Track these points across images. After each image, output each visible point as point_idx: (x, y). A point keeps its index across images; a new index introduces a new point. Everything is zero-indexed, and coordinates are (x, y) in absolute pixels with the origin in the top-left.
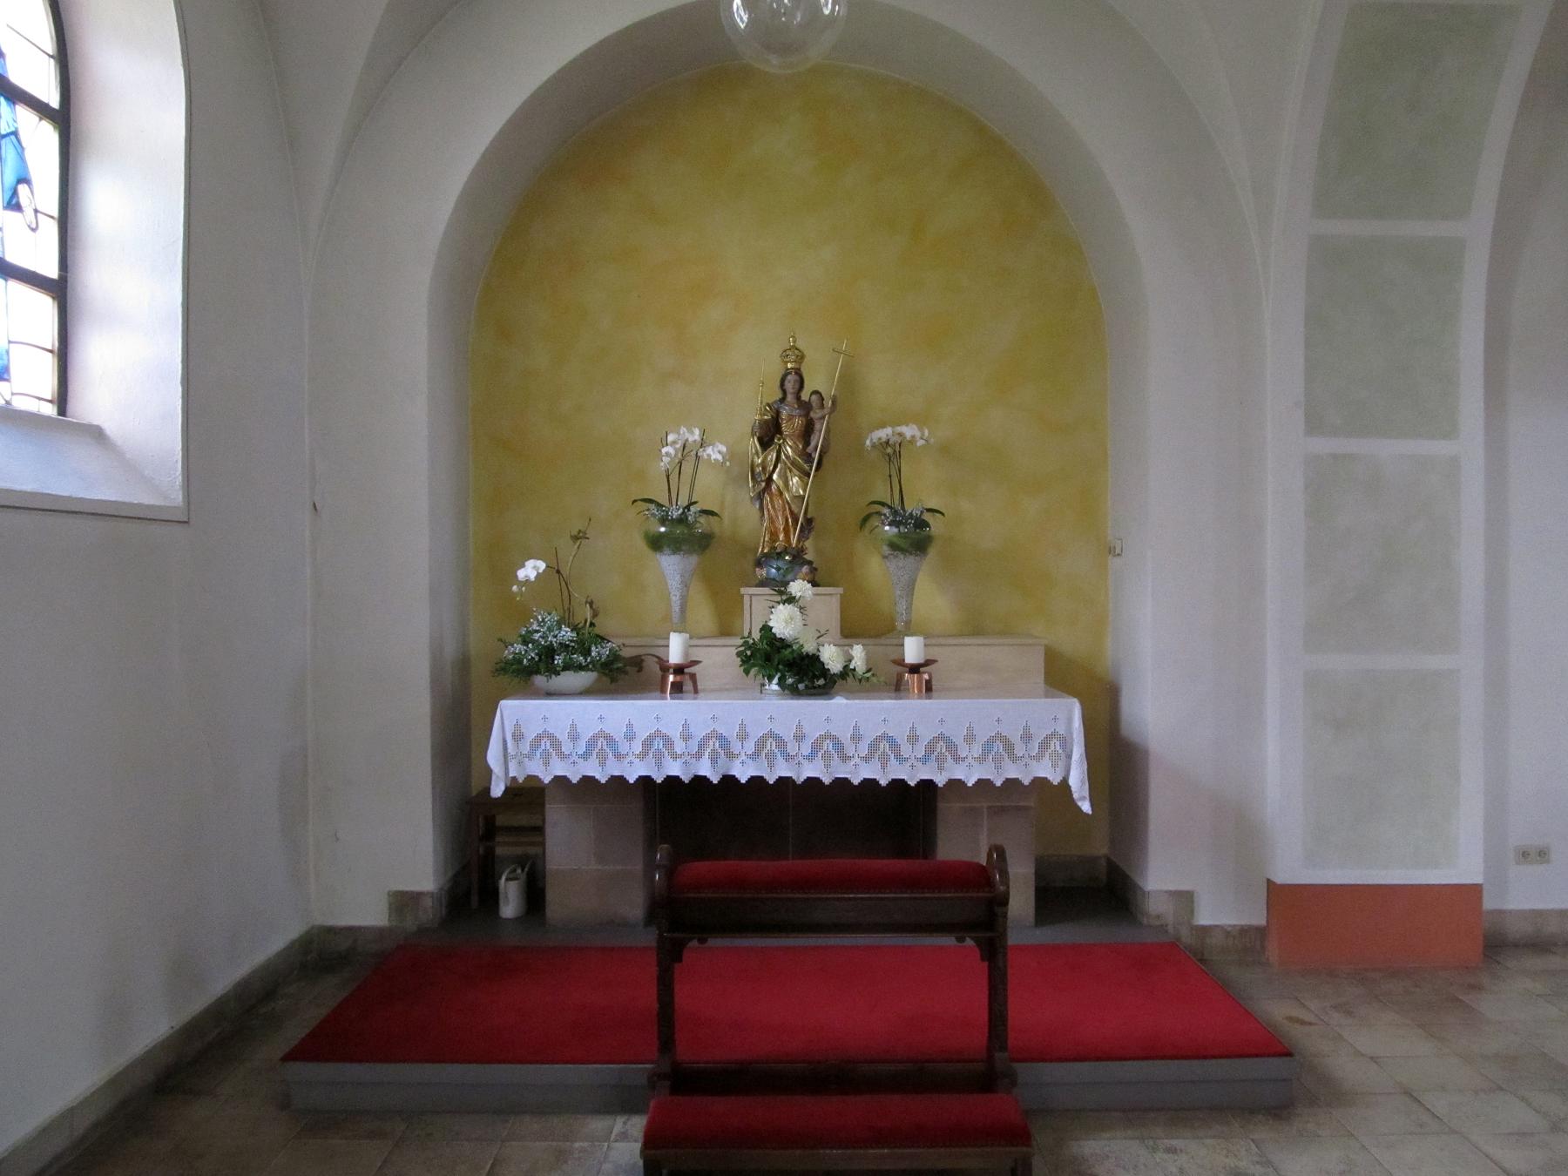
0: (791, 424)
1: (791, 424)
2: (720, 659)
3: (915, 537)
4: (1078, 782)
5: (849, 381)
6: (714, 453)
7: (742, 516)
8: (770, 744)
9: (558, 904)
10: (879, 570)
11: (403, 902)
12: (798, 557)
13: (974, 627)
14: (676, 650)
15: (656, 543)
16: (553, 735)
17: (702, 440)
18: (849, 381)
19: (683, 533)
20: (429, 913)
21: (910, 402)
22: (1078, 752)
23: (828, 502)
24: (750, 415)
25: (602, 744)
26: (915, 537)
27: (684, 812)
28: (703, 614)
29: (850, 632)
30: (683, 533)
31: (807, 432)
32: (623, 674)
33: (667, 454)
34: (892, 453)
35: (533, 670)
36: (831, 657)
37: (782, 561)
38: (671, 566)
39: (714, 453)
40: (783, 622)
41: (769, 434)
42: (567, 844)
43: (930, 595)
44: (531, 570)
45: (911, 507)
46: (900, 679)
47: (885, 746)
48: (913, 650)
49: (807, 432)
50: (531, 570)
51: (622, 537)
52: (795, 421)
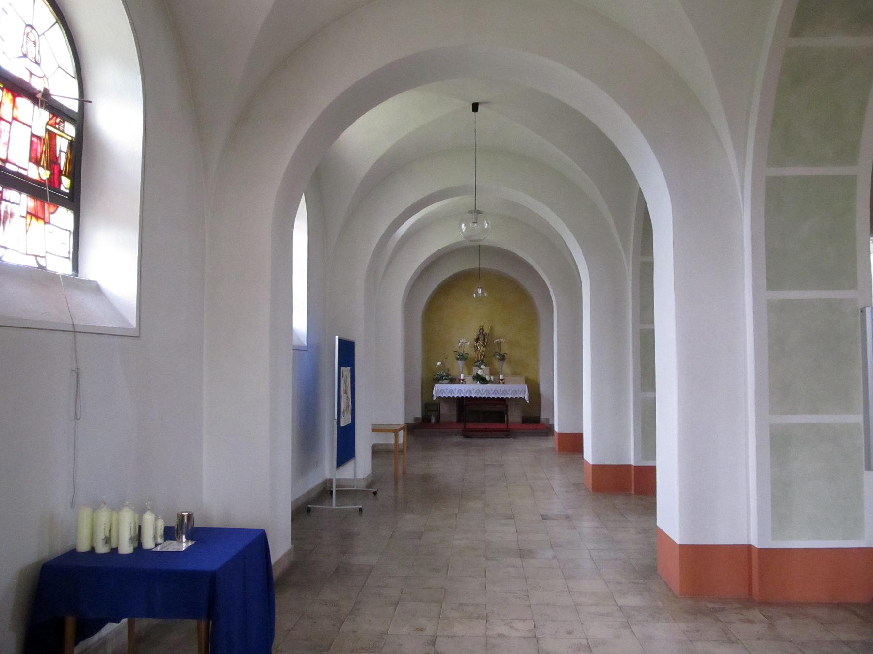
0: (481, 338)
1: (481, 338)
2: (470, 378)
3: (503, 358)
4: (527, 398)
5: (492, 329)
6: (468, 344)
7: (472, 353)
8: (478, 391)
9: (442, 420)
10: (497, 364)
11: (416, 419)
12: (482, 361)
13: (515, 374)
14: (462, 377)
15: (458, 359)
16: (442, 390)
17: (465, 341)
18: (492, 329)
19: (462, 357)
20: (421, 421)
21: (505, 334)
22: (527, 392)
23: (488, 353)
24: (474, 335)
25: (451, 391)
26: (503, 358)
27: (462, 404)
28: (465, 371)
29: (491, 374)
30: (462, 357)
31: (484, 339)
32: (453, 381)
33: (482, 293)
34: (499, 344)
35: (439, 379)
36: (488, 378)
37: (479, 362)
38: (460, 363)
39: (468, 344)
40: (480, 372)
41: (477, 340)
42: (444, 409)
43: (506, 368)
44: (439, 364)
45: (502, 353)
46: (498, 381)
47: (496, 392)
48: (501, 377)
49: (484, 339)
50: (439, 364)
51: (452, 357)
52: (482, 337)
